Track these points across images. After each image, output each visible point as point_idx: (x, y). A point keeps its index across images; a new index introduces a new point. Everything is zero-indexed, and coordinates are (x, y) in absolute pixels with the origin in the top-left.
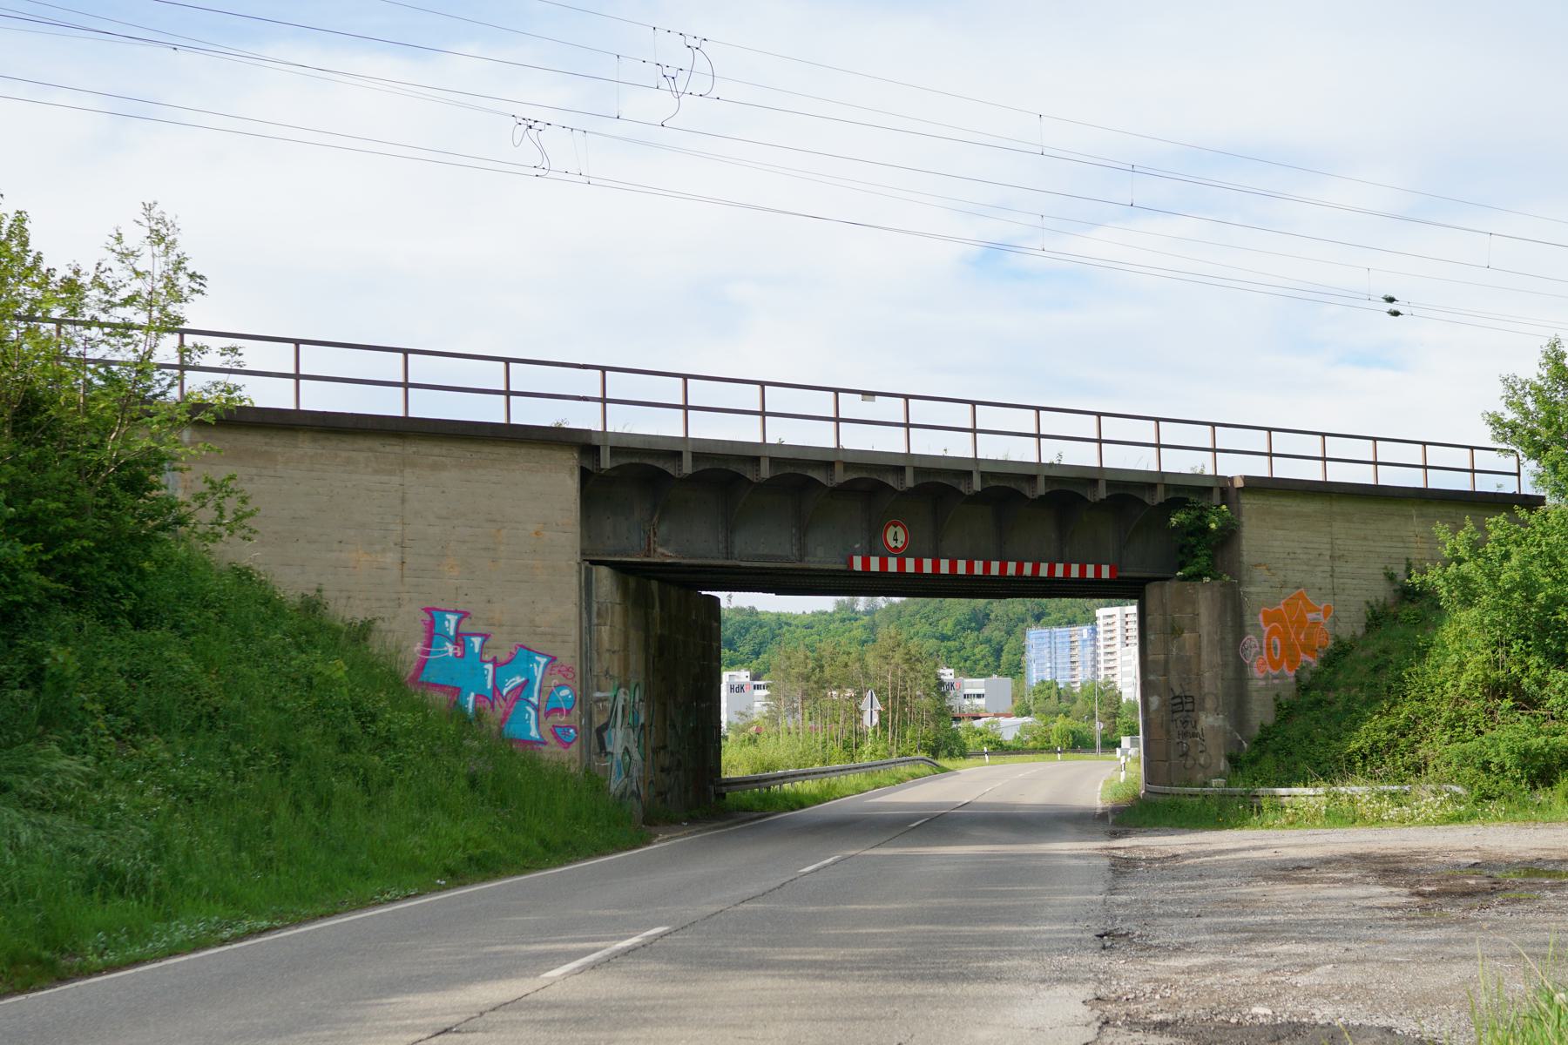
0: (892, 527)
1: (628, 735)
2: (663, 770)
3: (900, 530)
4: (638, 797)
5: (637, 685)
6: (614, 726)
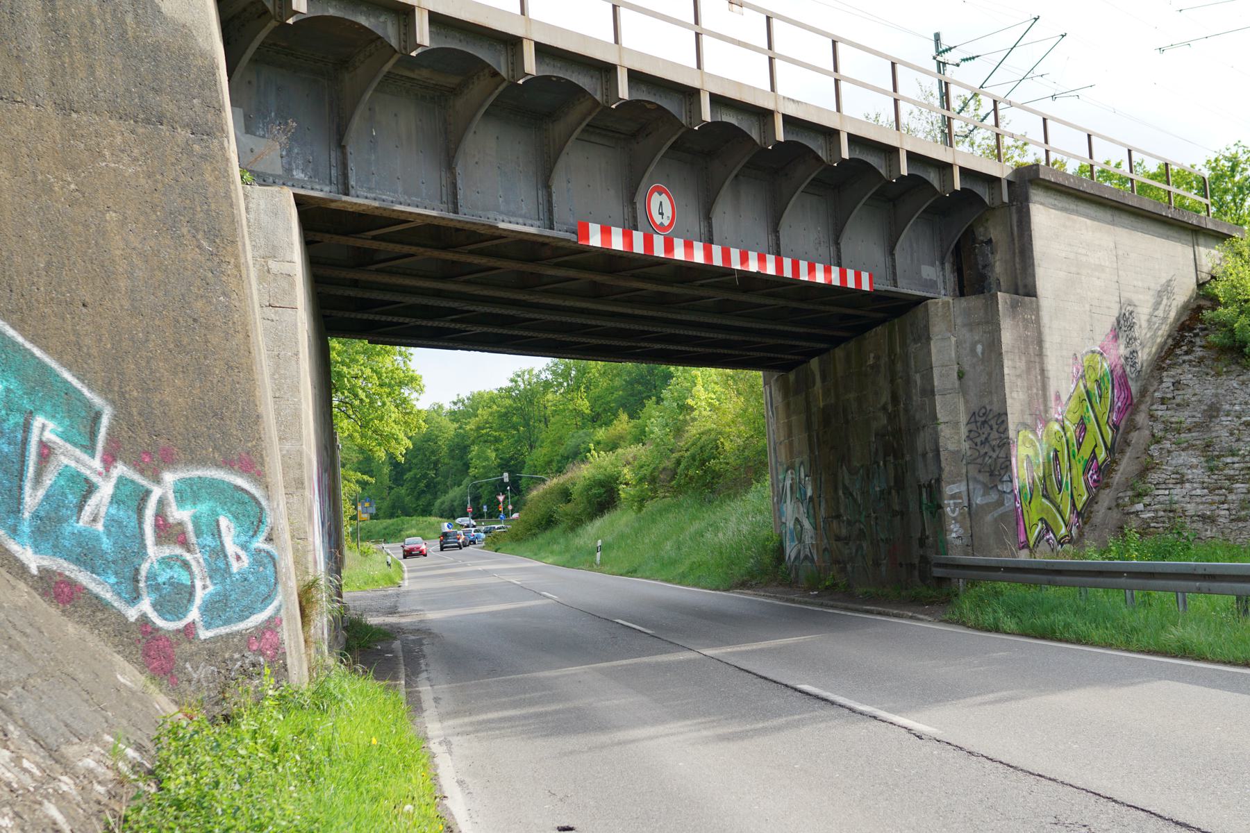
0: (656, 194)
1: (798, 508)
2: (838, 539)
3: (664, 197)
4: (812, 560)
5: (802, 463)
6: (785, 502)
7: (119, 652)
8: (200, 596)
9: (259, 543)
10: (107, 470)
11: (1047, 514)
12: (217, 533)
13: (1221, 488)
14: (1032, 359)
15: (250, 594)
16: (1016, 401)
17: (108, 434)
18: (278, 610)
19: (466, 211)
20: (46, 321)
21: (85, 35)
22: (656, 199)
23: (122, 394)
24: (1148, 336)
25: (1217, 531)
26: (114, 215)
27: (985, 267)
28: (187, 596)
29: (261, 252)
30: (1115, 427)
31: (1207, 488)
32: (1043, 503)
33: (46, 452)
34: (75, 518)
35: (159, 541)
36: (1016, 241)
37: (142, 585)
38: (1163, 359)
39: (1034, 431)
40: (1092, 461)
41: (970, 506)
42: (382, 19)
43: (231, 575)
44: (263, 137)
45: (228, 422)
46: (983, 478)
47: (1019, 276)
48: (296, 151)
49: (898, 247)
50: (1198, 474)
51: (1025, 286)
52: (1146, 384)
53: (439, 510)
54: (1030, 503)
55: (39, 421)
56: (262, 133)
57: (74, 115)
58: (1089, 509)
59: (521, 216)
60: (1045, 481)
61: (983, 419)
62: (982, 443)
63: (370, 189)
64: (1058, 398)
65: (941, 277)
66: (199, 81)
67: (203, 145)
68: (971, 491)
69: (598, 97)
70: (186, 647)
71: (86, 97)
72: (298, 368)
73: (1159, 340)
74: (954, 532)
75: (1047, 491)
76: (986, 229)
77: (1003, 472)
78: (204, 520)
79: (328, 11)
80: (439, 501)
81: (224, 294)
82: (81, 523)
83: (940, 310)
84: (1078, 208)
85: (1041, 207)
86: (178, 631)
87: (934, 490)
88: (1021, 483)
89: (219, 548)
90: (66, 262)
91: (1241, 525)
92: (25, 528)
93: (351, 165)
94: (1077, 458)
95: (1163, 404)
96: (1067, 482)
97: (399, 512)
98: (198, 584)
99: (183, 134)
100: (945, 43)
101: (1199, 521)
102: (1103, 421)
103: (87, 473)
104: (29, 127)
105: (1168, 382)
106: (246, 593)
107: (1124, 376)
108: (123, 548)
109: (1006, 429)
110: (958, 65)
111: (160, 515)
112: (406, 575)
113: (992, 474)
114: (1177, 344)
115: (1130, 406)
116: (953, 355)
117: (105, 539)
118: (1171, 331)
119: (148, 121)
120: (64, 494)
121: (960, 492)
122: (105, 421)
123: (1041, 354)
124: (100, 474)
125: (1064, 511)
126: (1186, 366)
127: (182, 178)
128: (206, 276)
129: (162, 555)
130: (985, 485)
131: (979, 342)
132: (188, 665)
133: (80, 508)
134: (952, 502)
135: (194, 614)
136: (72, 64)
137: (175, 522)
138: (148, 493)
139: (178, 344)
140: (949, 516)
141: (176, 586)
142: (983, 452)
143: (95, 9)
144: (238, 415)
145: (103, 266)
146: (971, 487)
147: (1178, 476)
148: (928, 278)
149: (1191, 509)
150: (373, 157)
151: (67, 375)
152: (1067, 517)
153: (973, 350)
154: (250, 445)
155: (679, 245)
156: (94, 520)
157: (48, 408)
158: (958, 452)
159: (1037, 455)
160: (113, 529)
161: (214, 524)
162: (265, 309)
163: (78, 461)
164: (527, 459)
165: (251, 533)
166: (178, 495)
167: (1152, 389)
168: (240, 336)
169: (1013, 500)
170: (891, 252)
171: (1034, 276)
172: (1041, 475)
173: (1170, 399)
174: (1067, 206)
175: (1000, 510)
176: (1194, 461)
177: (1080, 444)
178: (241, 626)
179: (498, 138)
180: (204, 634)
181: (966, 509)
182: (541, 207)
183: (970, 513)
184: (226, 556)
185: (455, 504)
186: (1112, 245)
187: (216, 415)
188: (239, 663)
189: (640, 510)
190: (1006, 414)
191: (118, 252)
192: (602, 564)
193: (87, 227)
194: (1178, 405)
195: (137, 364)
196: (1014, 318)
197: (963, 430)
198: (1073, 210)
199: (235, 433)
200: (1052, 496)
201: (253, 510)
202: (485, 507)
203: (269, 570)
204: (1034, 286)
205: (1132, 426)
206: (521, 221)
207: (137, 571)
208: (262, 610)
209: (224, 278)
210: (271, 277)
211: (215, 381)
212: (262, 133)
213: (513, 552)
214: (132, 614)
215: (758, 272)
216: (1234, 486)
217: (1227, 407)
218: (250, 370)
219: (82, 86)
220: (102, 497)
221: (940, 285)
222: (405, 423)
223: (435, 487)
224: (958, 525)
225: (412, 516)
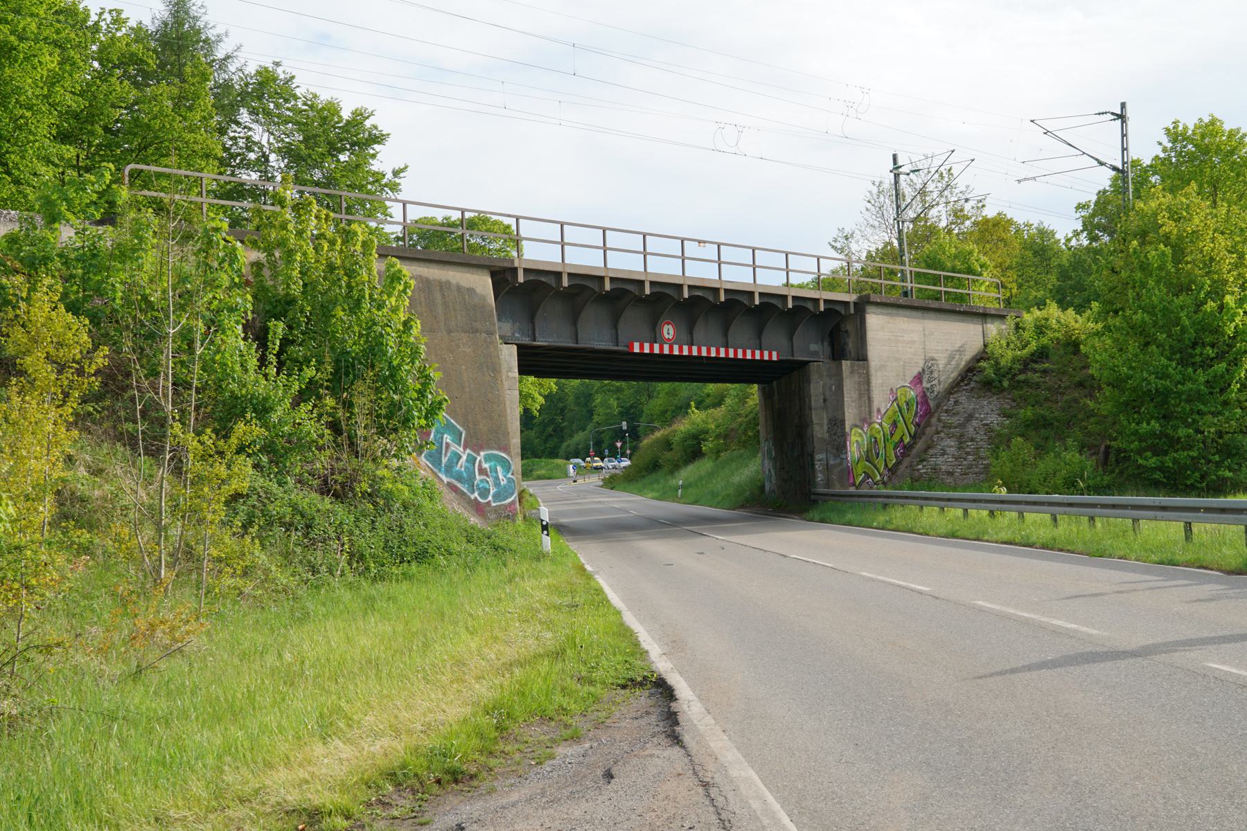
3: (670, 326)
12: (496, 472)
15: (269, 568)
16: (850, 414)
22: (666, 327)
23: (468, 426)
30: (918, 425)
33: (448, 445)
35: (480, 474)
38: (953, 388)
39: (862, 429)
41: (827, 465)
49: (795, 337)
50: (951, 450)
53: (565, 452)
55: (445, 436)
63: (543, 338)
64: (879, 411)
69: (637, 293)
74: (820, 477)
85: (874, 316)
87: (812, 456)
92: (443, 469)
93: (537, 329)
97: (529, 453)
99: (484, 335)
100: (900, 163)
102: (909, 423)
105: (952, 401)
106: (506, 491)
109: (845, 428)
111: (480, 465)
112: (541, 504)
113: (838, 450)
114: (962, 380)
115: (928, 413)
116: (821, 390)
122: (463, 435)
123: (869, 390)
126: (964, 392)
135: (490, 498)
138: (476, 458)
141: (485, 489)
153: (831, 388)
155: (676, 348)
159: (863, 440)
164: (645, 409)
170: (791, 339)
171: (866, 350)
175: (841, 467)
176: (953, 444)
177: (892, 435)
183: (827, 468)
185: (580, 447)
186: (921, 329)
189: (716, 459)
192: (682, 497)
197: (825, 427)
202: (606, 451)
203: (513, 485)
204: (867, 355)
205: (928, 424)
213: (625, 490)
217: (977, 415)
221: (821, 353)
222: (540, 384)
225: (540, 458)
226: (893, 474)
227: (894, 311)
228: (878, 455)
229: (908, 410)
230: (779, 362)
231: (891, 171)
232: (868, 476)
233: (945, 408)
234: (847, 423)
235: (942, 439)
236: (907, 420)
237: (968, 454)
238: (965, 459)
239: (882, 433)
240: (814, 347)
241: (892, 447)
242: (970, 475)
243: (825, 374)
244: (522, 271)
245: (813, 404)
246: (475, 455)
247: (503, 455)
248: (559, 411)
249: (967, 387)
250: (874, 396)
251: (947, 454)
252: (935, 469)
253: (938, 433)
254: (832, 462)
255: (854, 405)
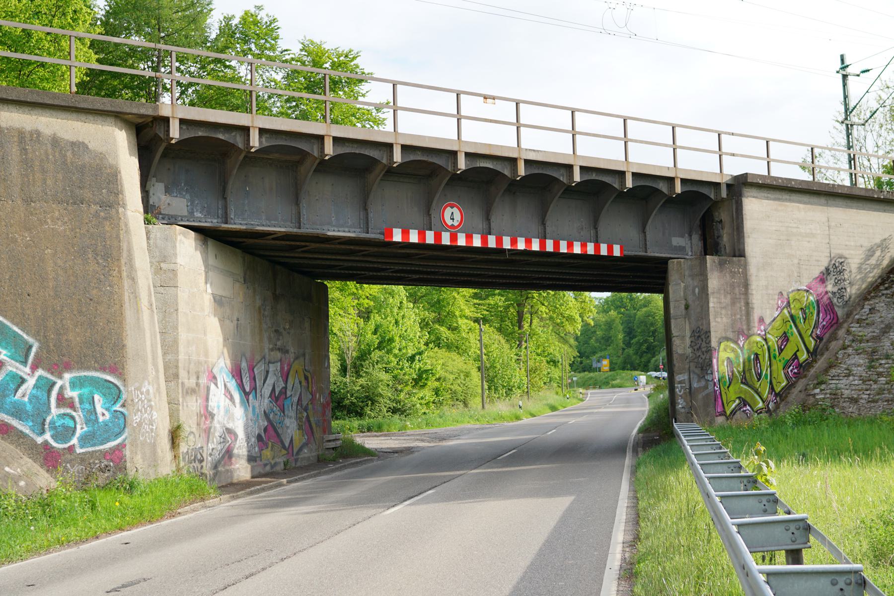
3: (455, 210)
7: (30, 458)
8: (79, 432)
9: (117, 407)
10: (33, 373)
11: (745, 394)
12: (93, 402)
13: (870, 380)
14: (738, 297)
17: (35, 356)
18: (124, 440)
19: (307, 226)
20: (7, 303)
21: (43, 164)
22: (448, 212)
24: (858, 277)
25: (856, 409)
26: (50, 251)
27: (718, 237)
28: (72, 432)
29: (157, 259)
30: (819, 338)
31: (862, 380)
32: (742, 387)
34: (13, 395)
36: (735, 222)
37: (46, 426)
38: (869, 293)
39: (736, 342)
40: (793, 360)
42: (233, 134)
43: (98, 422)
44: (176, 196)
45: (105, 349)
46: (698, 371)
47: (736, 244)
48: (197, 202)
51: (739, 250)
52: (853, 309)
54: (728, 387)
56: (175, 195)
57: (33, 204)
58: (787, 391)
59: (347, 227)
60: (744, 373)
61: (698, 335)
62: (698, 350)
63: (243, 219)
64: (761, 320)
65: (689, 244)
66: (107, 180)
67: (106, 212)
68: (692, 379)
70: (68, 456)
71: (40, 195)
72: (178, 317)
73: (870, 280)
75: (745, 379)
76: (719, 213)
77: (708, 368)
78: (85, 396)
79: (198, 134)
80: (654, 359)
81: (110, 286)
82: (16, 397)
83: (675, 266)
84: (791, 198)
86: (65, 449)
88: (720, 376)
89: (93, 410)
90: (21, 275)
91: (872, 405)
94: (777, 359)
95: (858, 323)
96: (766, 375)
97: (629, 366)
98: (78, 427)
99: (94, 208)
100: (847, 62)
101: (848, 401)
103: (22, 374)
104: (7, 212)
105: (867, 309)
107: (831, 305)
108: (38, 409)
109: (710, 341)
110: (858, 75)
114: (882, 283)
115: (835, 323)
117: (28, 405)
118: (882, 273)
119: (75, 203)
120: (8, 384)
121: (684, 380)
122: (34, 350)
124: (29, 374)
125: (762, 392)
126: (883, 298)
127: (92, 230)
128: (100, 278)
129: (59, 413)
130: (698, 375)
131: (697, 286)
132: (68, 465)
133: (16, 391)
134: (679, 385)
135: (74, 441)
136: (34, 180)
137: (68, 397)
138: (54, 384)
139: (80, 312)
140: (678, 394)
142: (698, 355)
143: (50, 151)
144: (111, 345)
145: (41, 276)
146: (692, 376)
147: (848, 372)
148: (678, 245)
149: (846, 393)
150: (246, 202)
151: (15, 329)
152: (765, 396)
153: (694, 291)
154: (116, 360)
156: (23, 396)
157: (3, 344)
158: (684, 354)
159: (737, 357)
160: (33, 400)
161: (91, 398)
162: (158, 288)
163: (17, 368)
165: (112, 403)
166: (72, 384)
167: (855, 313)
168: (117, 307)
169: (713, 386)
171: (744, 244)
172: (741, 369)
173: (864, 320)
174: (781, 197)
175: (706, 392)
176: (861, 361)
177: (781, 350)
178: (101, 447)
179: (333, 185)
180: (79, 450)
181: (688, 390)
182: (361, 221)
184: (96, 414)
187: (98, 345)
188: (98, 465)
190: (710, 332)
191: (50, 269)
193: (34, 257)
194: (867, 324)
195: (55, 322)
196: (721, 272)
197: (688, 341)
198: (786, 199)
199: (108, 354)
200: (750, 383)
201: (114, 391)
203: (122, 421)
205: (834, 337)
206: (347, 229)
207: (44, 420)
208: (114, 440)
209: (111, 278)
210: (162, 272)
211: (99, 329)
212: (175, 195)
214: (40, 440)
215: (525, 250)
216: (879, 379)
218: (121, 323)
219: (39, 190)
220: (29, 386)
223: (653, 349)
224: (682, 400)
226: (782, 400)
227: (786, 196)
228: (759, 376)
229: (805, 319)
230: (623, 259)
231: (838, 72)
232: (744, 402)
233: (857, 317)
234: (713, 334)
235: (849, 355)
236: (803, 332)
237: (880, 374)
238: (876, 382)
239: (766, 347)
240: (677, 241)
241: (781, 366)
242: (880, 403)
243: (687, 273)
244: (177, 123)
245: (672, 312)
246: (53, 378)
247: (109, 378)
248: (651, 334)
249: (888, 292)
250: (754, 301)
251: (853, 375)
252: (835, 396)
253: (844, 348)
254: (695, 385)
255: (723, 312)
